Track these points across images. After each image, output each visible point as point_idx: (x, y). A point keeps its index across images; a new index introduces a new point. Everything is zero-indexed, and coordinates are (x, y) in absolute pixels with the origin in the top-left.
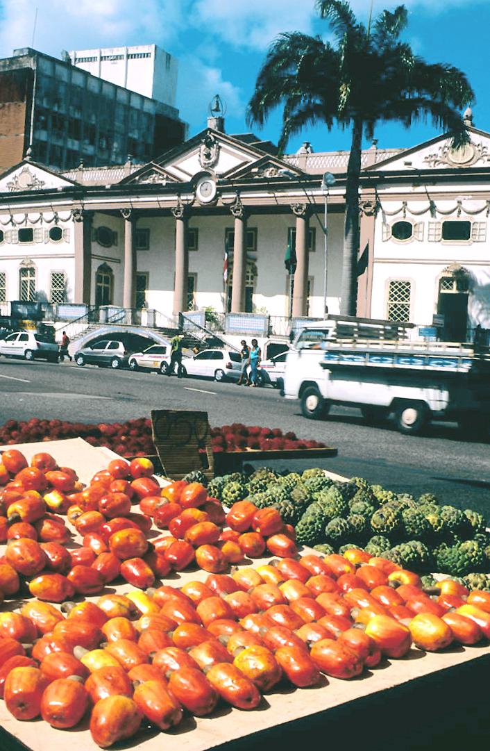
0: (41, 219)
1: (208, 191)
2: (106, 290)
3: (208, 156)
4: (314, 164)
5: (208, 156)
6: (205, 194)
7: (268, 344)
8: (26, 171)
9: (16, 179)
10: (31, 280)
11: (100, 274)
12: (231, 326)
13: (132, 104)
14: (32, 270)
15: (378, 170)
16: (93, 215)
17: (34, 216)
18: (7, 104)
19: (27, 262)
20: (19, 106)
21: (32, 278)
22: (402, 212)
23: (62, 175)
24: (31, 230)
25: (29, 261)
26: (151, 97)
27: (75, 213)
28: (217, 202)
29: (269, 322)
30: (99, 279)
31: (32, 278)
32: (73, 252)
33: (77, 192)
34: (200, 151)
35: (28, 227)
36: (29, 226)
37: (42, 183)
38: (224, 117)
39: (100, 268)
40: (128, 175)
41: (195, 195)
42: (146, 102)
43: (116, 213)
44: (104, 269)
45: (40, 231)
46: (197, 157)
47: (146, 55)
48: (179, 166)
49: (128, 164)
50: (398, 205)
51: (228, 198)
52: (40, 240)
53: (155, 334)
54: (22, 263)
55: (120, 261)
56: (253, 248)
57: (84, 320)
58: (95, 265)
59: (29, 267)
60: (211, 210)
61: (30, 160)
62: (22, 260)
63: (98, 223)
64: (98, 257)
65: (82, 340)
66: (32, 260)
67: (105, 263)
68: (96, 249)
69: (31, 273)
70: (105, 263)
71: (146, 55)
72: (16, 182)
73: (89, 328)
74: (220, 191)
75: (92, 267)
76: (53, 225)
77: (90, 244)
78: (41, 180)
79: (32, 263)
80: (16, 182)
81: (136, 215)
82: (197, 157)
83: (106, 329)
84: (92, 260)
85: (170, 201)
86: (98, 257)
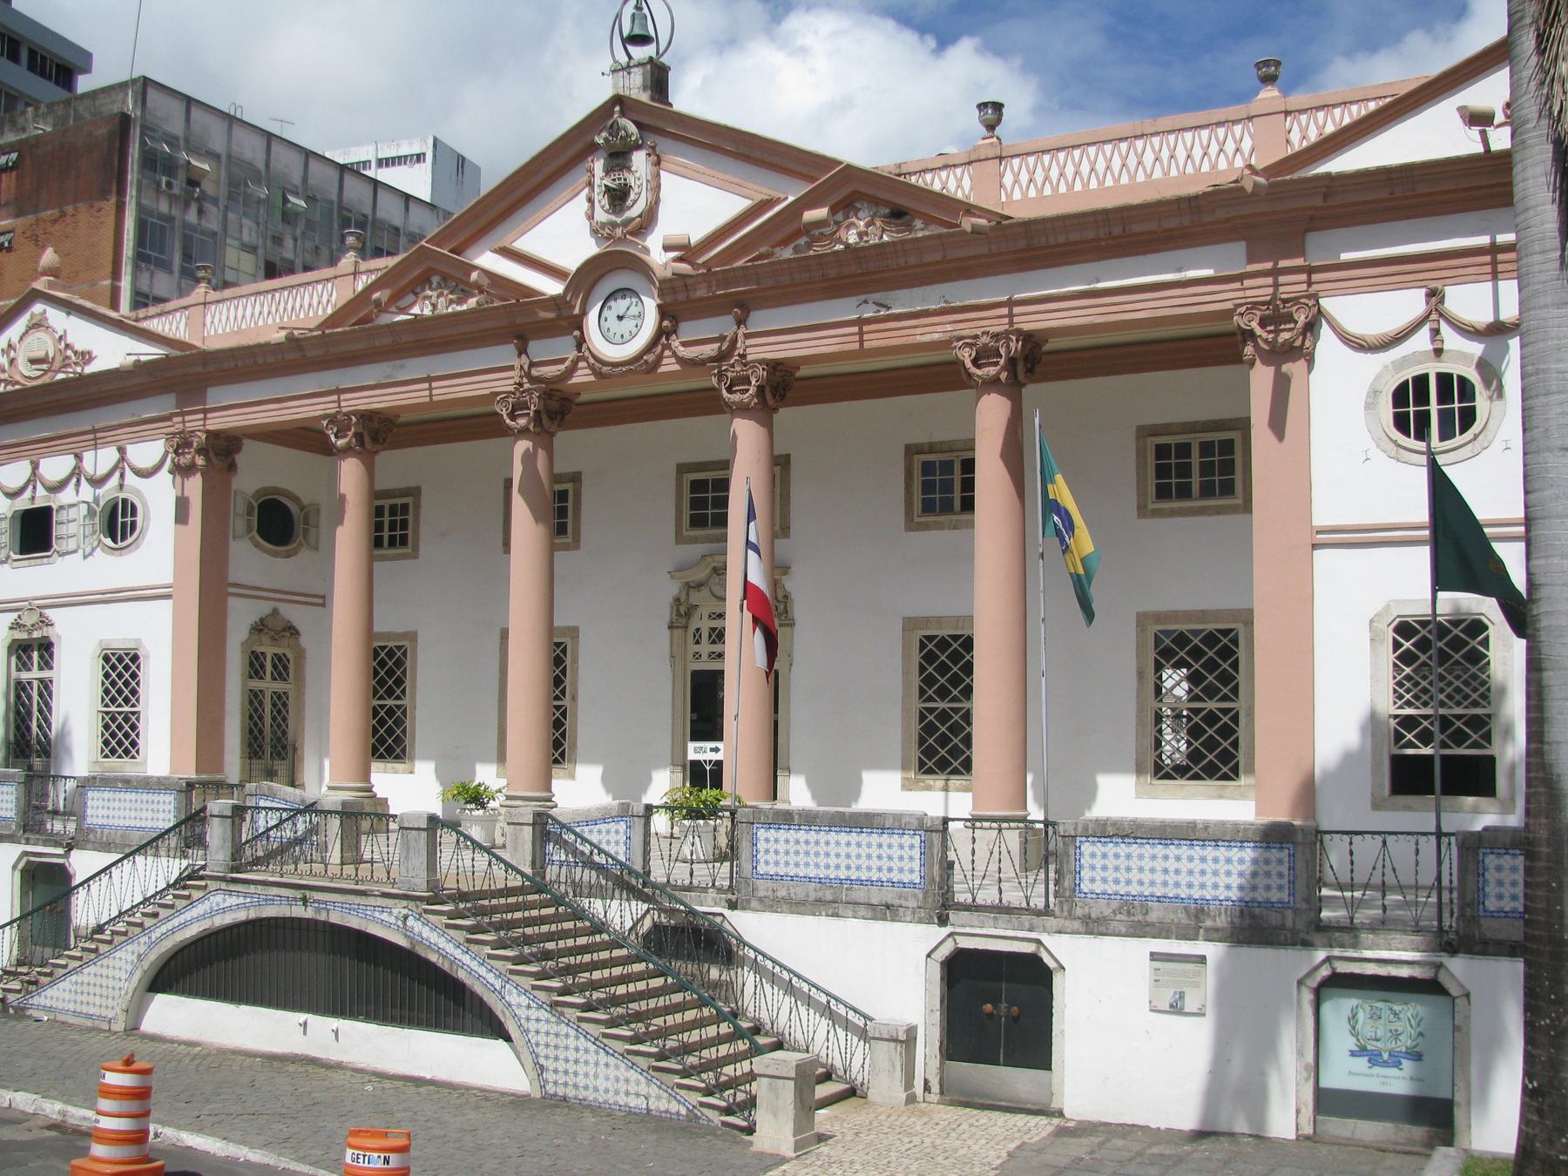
0: (77, 472)
1: (628, 324)
2: (280, 701)
3: (619, 197)
4: (1047, 178)
5: (619, 197)
6: (620, 332)
7: (946, 950)
8: (38, 325)
9: (12, 354)
10: (41, 680)
11: (259, 649)
12: (762, 869)
13: (380, 214)
14: (46, 647)
15: (1322, 169)
16: (238, 449)
17: (56, 467)
18: (70, 209)
19: (29, 619)
20: (99, 210)
21: (45, 674)
22: (1424, 333)
23: (144, 325)
24: (47, 512)
25: (35, 618)
26: (428, 200)
27: (181, 444)
28: (660, 358)
29: (945, 848)
30: (255, 666)
31: (45, 674)
32: (169, 580)
33: (184, 376)
34: (590, 184)
35: (39, 504)
36: (42, 498)
37: (86, 357)
38: (664, 60)
39: (259, 628)
40: (350, 296)
41: (581, 342)
42: (413, 206)
43: (306, 438)
44: (274, 628)
45: (73, 513)
46: (580, 203)
47: (420, 158)
48: (524, 244)
49: (348, 260)
50: (1408, 303)
51: (700, 337)
52: (72, 544)
53: (434, 928)
54: (16, 626)
55: (322, 600)
56: (1239, 501)
57: (173, 841)
58: (241, 617)
59: (36, 635)
60: (633, 401)
61: (51, 285)
62: (15, 615)
63: (260, 471)
64: (251, 592)
65: (140, 945)
66: (48, 612)
67: (275, 612)
68: (250, 560)
69: (41, 657)
70: (275, 612)
71: (420, 158)
72: (12, 361)
73: (180, 883)
74: (671, 316)
75: (231, 622)
76: (109, 490)
77: (227, 545)
78: (79, 347)
79: (46, 623)
80: (12, 361)
81: (379, 433)
82: (580, 203)
83: (233, 900)
84: (232, 601)
85: (486, 376)
86: (251, 592)
